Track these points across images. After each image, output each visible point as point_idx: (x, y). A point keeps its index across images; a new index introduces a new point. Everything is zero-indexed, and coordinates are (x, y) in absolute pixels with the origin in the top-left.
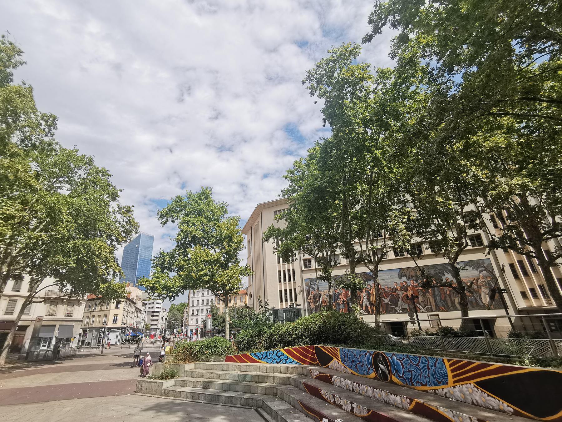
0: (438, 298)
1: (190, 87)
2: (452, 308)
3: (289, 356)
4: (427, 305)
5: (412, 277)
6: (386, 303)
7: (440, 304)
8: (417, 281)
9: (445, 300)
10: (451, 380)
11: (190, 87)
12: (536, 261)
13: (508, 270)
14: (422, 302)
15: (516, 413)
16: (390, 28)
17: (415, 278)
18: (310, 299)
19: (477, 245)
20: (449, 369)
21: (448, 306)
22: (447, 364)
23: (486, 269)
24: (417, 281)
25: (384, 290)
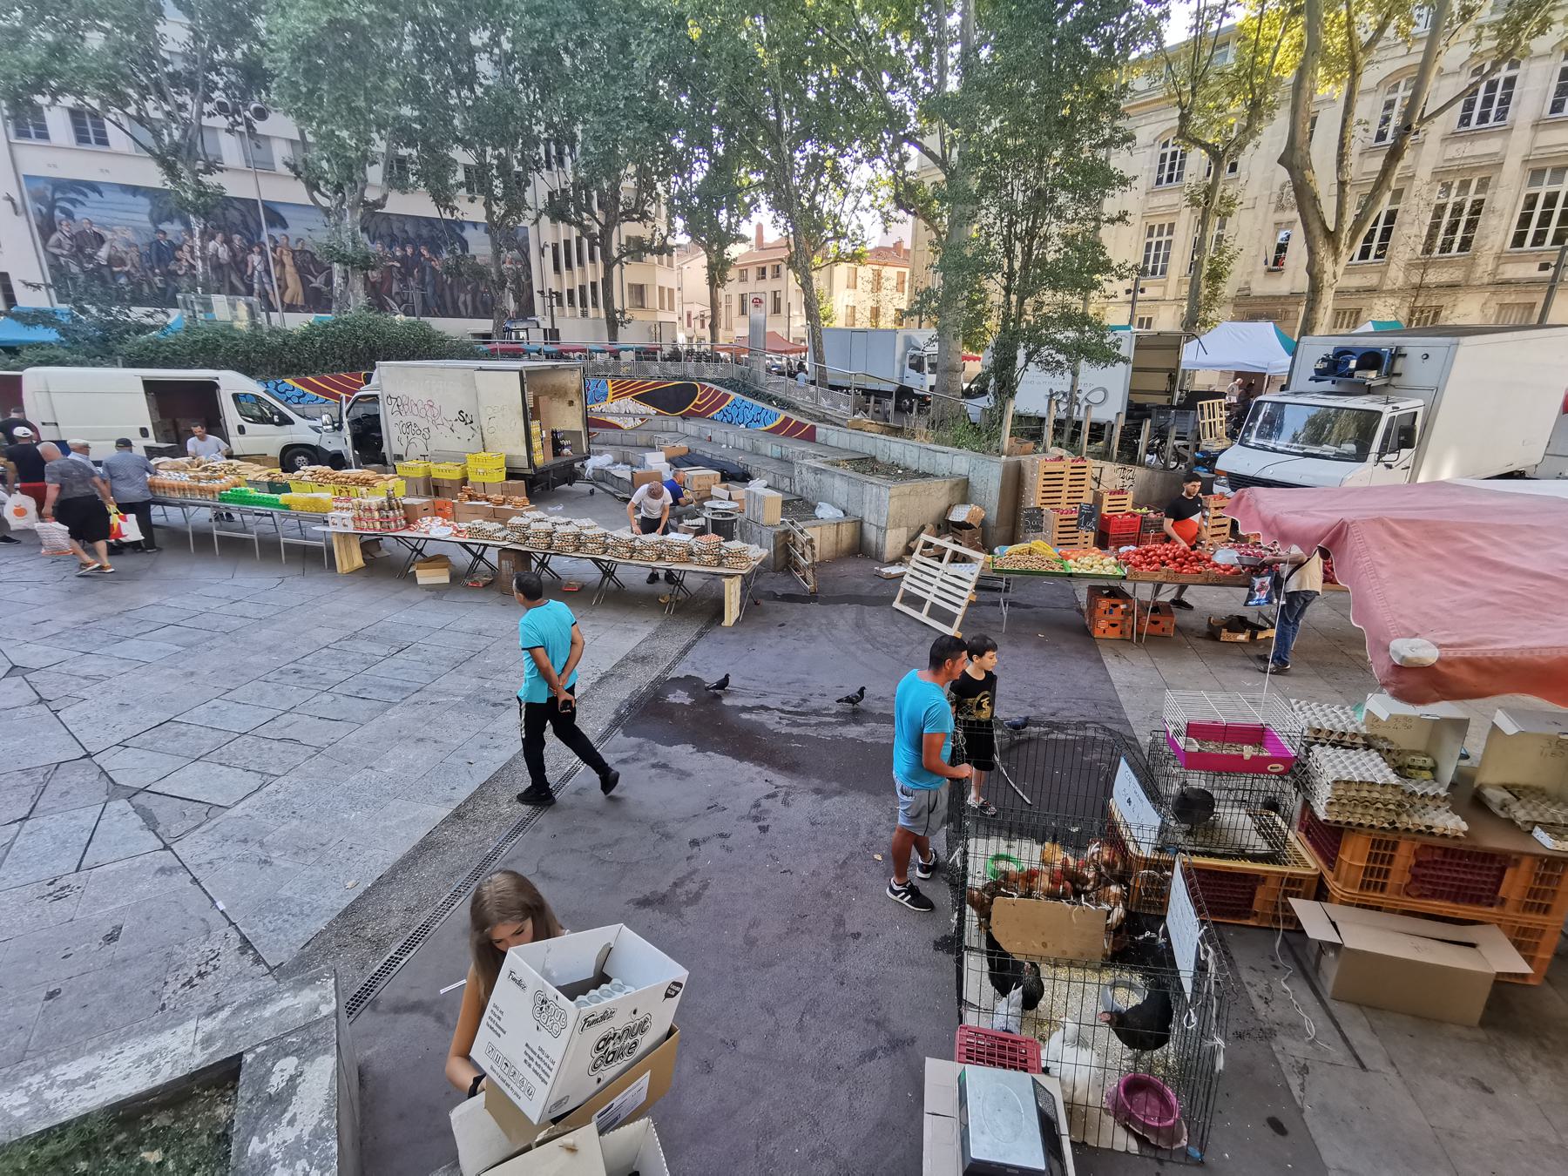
0: (429, 290)
1: (689, 775)
2: (451, 312)
3: (306, 390)
4: (406, 302)
5: (381, 237)
6: (315, 288)
7: (431, 302)
8: (391, 248)
9: (441, 296)
10: (610, 396)
11: (689, 775)
12: (598, 249)
13: (549, 252)
14: (397, 293)
15: (658, 413)
16: (572, 1150)
17: (387, 240)
18: (60, 246)
19: (33, 135)
20: (610, 388)
21: (445, 307)
22: (610, 384)
23: (519, 248)
24: (391, 248)
25: (312, 255)
